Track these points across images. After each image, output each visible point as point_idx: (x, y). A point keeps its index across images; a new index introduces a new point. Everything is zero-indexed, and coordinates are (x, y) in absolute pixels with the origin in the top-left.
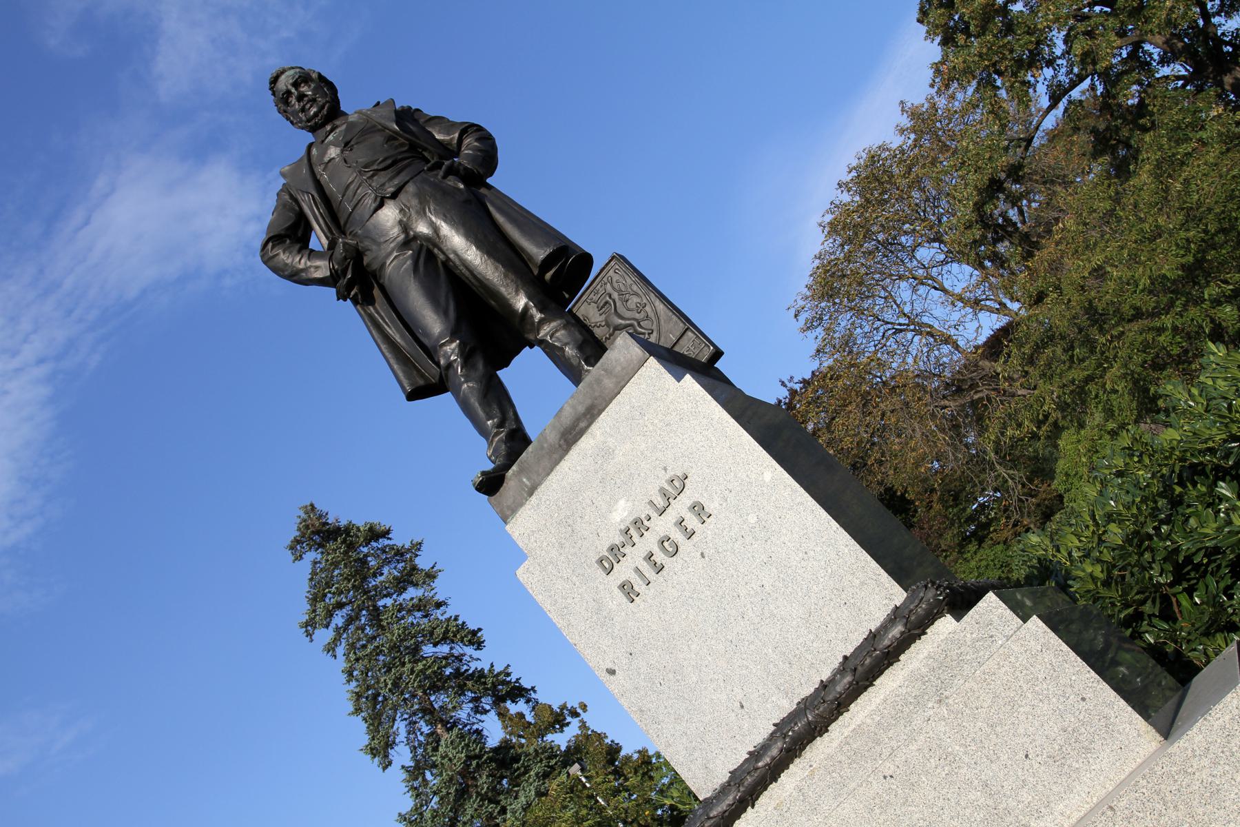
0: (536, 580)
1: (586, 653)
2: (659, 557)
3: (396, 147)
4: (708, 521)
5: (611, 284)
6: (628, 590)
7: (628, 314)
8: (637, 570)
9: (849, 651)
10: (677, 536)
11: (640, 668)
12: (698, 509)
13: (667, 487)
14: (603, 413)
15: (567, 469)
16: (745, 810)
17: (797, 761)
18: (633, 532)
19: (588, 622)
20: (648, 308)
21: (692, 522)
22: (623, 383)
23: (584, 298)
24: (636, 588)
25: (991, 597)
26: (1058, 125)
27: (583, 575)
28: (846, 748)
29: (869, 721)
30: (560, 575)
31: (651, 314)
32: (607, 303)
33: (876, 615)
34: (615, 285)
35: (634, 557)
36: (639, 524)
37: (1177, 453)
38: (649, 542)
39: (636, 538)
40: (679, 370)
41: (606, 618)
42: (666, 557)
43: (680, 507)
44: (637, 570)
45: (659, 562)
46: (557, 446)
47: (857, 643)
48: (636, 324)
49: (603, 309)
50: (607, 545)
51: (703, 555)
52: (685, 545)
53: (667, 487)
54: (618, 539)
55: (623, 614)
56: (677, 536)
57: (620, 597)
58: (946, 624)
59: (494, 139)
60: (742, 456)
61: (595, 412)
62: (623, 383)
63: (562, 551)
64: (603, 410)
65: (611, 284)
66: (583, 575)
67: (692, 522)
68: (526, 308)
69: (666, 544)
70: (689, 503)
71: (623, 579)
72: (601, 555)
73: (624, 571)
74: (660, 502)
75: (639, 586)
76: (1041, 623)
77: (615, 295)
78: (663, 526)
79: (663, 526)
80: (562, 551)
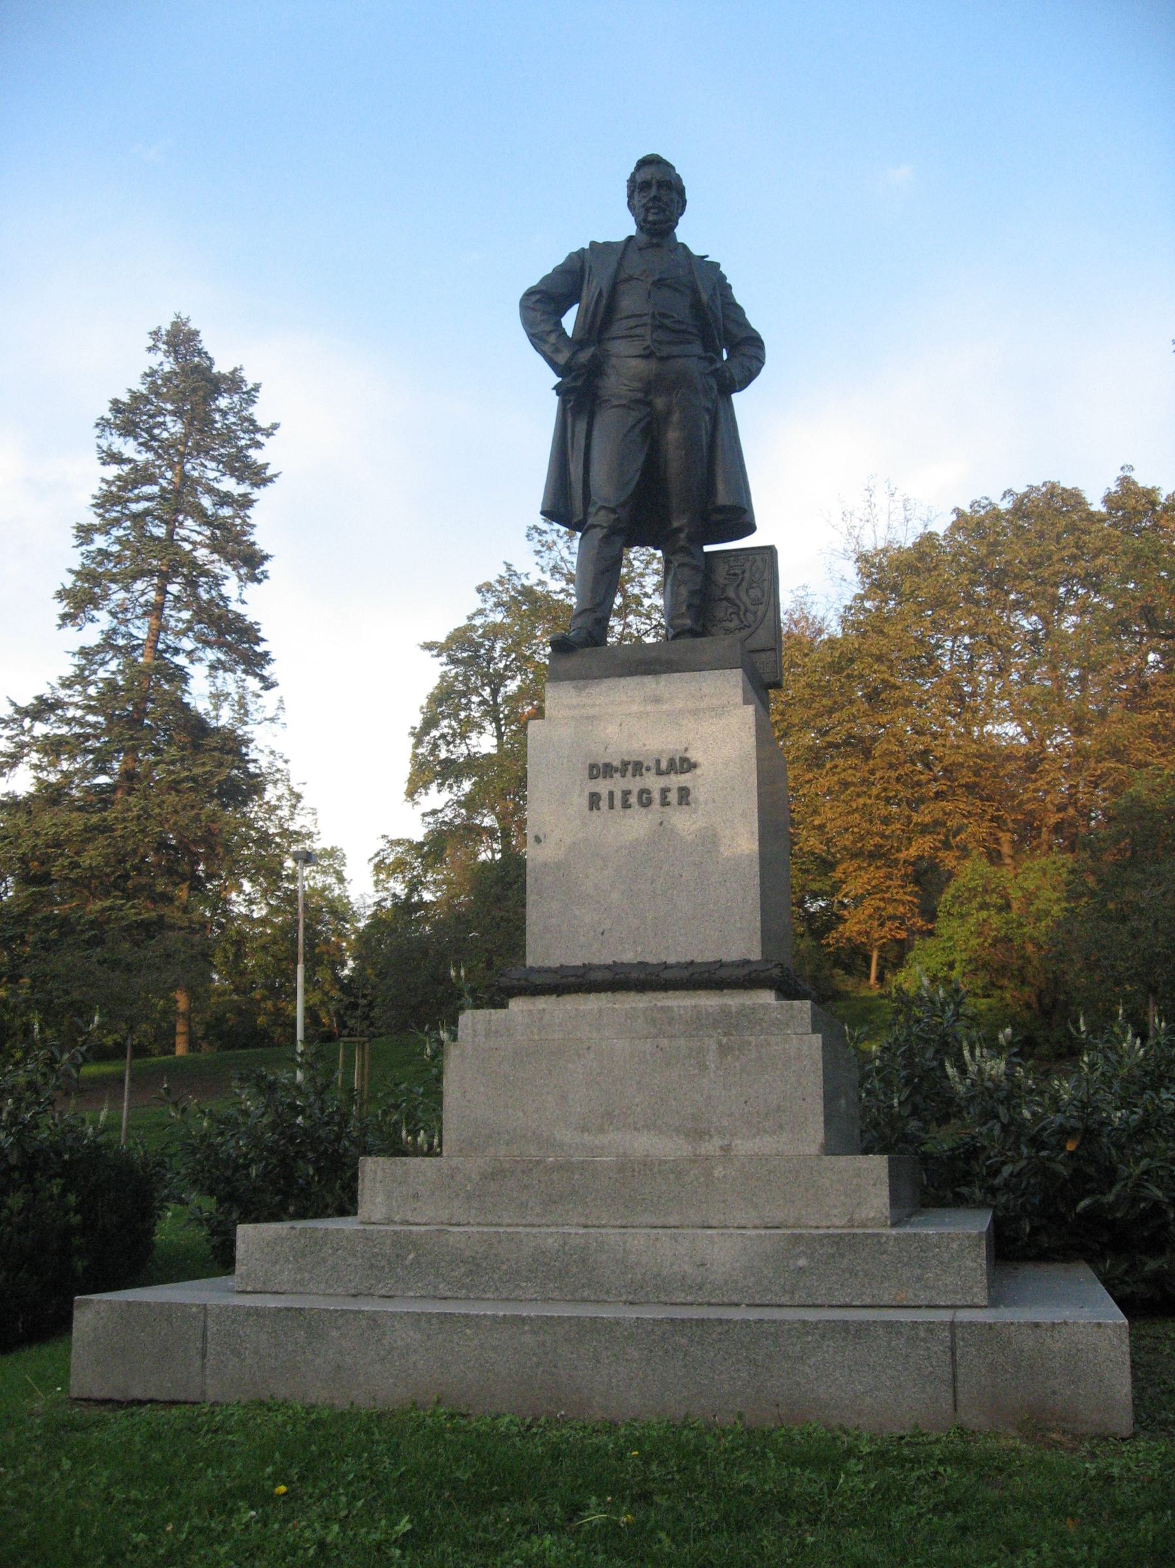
2: (633, 799)
6: (594, 801)
7: (744, 598)
8: (611, 794)
9: (699, 960)
10: (656, 796)
12: (684, 794)
13: (677, 761)
16: (551, 994)
17: (609, 994)
18: (630, 767)
21: (673, 797)
23: (924, 1297)
24: (601, 804)
25: (808, 1004)
26: (307, 858)
28: (649, 1012)
29: (676, 1009)
31: (759, 614)
32: (735, 574)
33: (733, 953)
34: (754, 568)
35: (617, 784)
36: (638, 768)
38: (634, 784)
39: (629, 773)
40: (752, 694)
43: (675, 781)
44: (611, 794)
45: (668, 799)
47: (705, 959)
48: (743, 608)
50: (607, 760)
51: (661, 824)
53: (677, 761)
54: (616, 763)
56: (656, 796)
57: (585, 802)
58: (767, 997)
59: (763, 363)
64: (678, 671)
67: (673, 797)
68: (679, 530)
69: (645, 796)
71: (597, 790)
73: (603, 787)
74: (664, 765)
75: (604, 804)
76: (820, 1040)
77: (747, 575)
78: (654, 783)
79: (654, 783)
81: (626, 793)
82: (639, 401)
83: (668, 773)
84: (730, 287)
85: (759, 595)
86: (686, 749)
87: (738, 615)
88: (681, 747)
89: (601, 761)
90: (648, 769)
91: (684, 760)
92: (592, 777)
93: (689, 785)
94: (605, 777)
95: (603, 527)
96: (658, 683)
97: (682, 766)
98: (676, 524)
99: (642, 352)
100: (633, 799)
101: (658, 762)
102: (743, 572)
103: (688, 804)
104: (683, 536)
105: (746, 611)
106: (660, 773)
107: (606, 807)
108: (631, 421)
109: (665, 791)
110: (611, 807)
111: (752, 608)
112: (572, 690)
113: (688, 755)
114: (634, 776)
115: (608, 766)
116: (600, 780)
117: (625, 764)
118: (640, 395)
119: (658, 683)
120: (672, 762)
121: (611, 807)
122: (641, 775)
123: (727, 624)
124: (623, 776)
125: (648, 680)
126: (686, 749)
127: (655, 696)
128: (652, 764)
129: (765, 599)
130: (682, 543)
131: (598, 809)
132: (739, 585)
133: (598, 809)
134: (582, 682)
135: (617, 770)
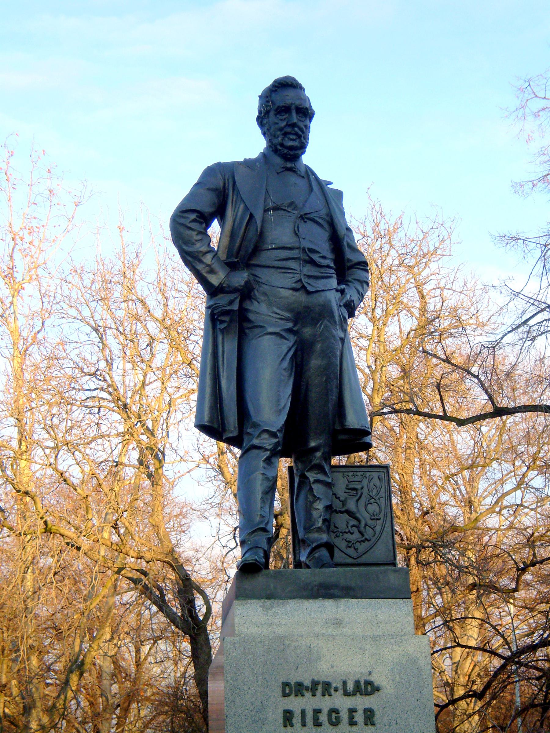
0: (234, 654)
1: (229, 728)
2: (323, 718)
3: (228, 180)
4: (370, 727)
5: (369, 482)
8: (303, 712)
10: (344, 716)
11: (13, 480)
12: (369, 714)
13: (362, 683)
14: (356, 600)
15: (305, 607)
18: (320, 687)
19: (247, 711)
20: (379, 522)
21: (359, 717)
22: (382, 595)
24: (294, 721)
27: (267, 682)
30: (253, 667)
31: (378, 528)
32: (356, 489)
37: (330, 630)
39: (319, 692)
41: (260, 719)
42: (327, 722)
44: (303, 712)
45: (356, 719)
46: (310, 588)
49: (350, 491)
50: (299, 679)
52: (344, 725)
53: (362, 683)
54: (307, 683)
55: (273, 728)
56: (344, 716)
60: (420, 711)
61: (352, 593)
62: (382, 595)
63: (266, 654)
64: (357, 597)
65: (369, 482)
66: (267, 682)
67: (359, 717)
69: (334, 715)
70: (367, 706)
72: (289, 681)
74: (350, 686)
75: (297, 720)
80: (266, 654)
81: (317, 712)
82: (290, 331)
83: (354, 695)
84: (245, 159)
85: (377, 510)
86: (370, 673)
87: (358, 527)
88: (366, 671)
89: (293, 679)
90: (336, 690)
91: (368, 683)
92: (285, 695)
93: (375, 707)
94: (296, 696)
95: (267, 450)
96: (338, 607)
97: (366, 688)
98: (313, 444)
99: (294, 285)
100: (323, 718)
101: (345, 683)
102: (362, 488)
103: (373, 724)
104: (319, 454)
105: (366, 525)
106: (346, 694)
107: (299, 725)
108: (285, 349)
109: (352, 711)
110: (304, 725)
111: (370, 522)
112: (260, 609)
113: (371, 678)
114: (323, 695)
115: (299, 685)
116: (292, 697)
117: (315, 683)
118: (290, 325)
119: (338, 607)
120: (357, 683)
121: (304, 725)
122: (330, 695)
123: (348, 536)
124: (314, 695)
125: (329, 604)
126: (370, 673)
127: (336, 619)
128: (340, 685)
129: (382, 516)
130: (316, 462)
131: (292, 726)
132: (358, 501)
133: (292, 726)
134: (268, 602)
135: (307, 689)
